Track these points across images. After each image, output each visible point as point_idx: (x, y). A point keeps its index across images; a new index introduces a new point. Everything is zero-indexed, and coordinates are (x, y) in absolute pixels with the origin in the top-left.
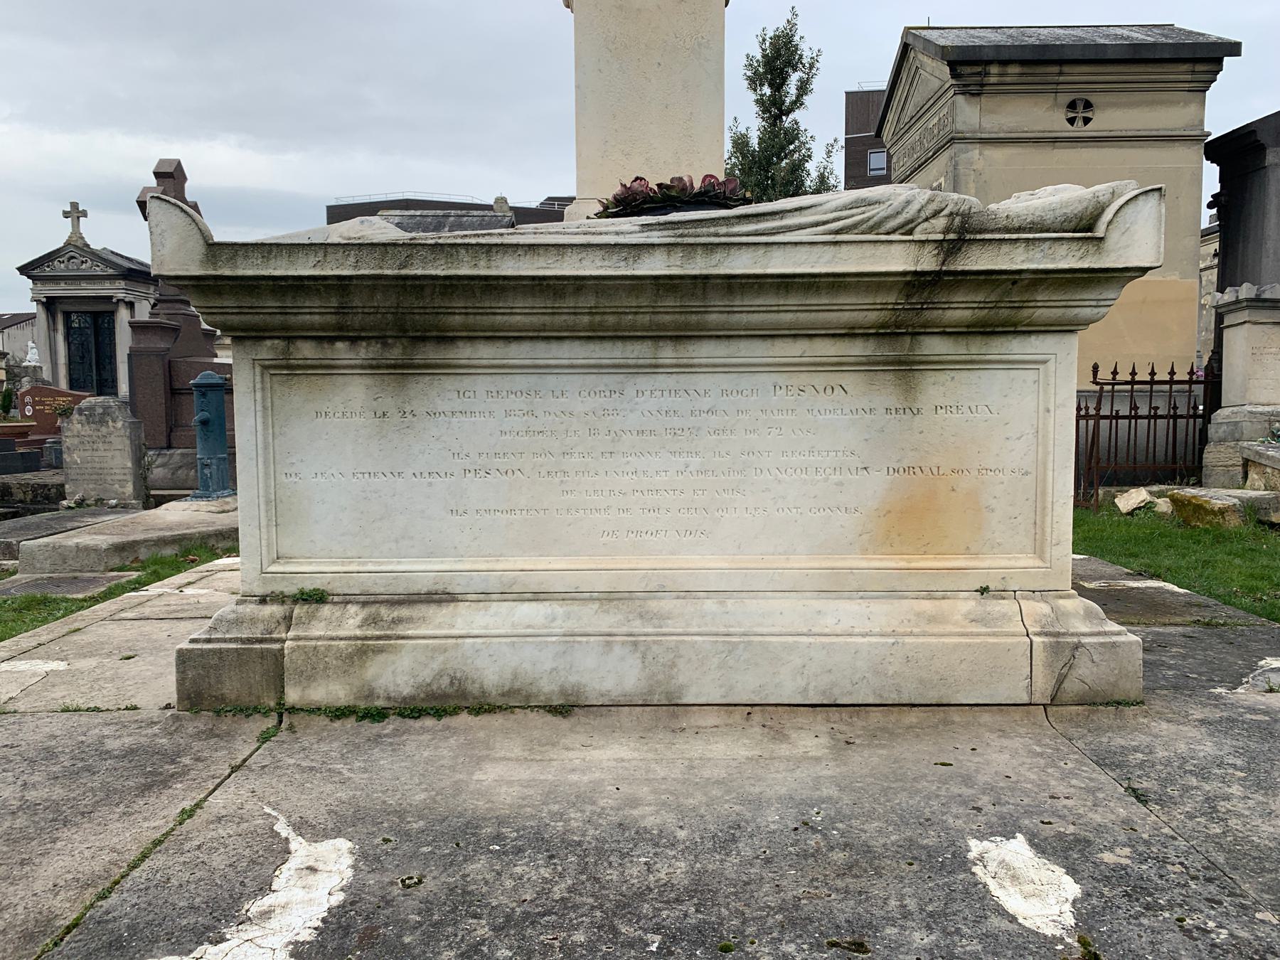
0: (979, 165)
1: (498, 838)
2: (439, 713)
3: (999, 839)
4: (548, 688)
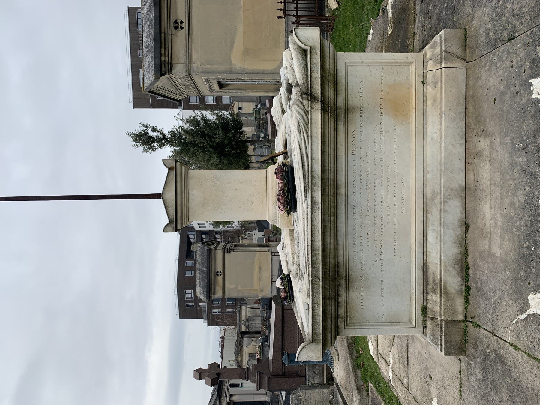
0: (199, 64)
1: (529, 248)
2: (468, 268)
3: (532, 88)
4: (459, 231)
